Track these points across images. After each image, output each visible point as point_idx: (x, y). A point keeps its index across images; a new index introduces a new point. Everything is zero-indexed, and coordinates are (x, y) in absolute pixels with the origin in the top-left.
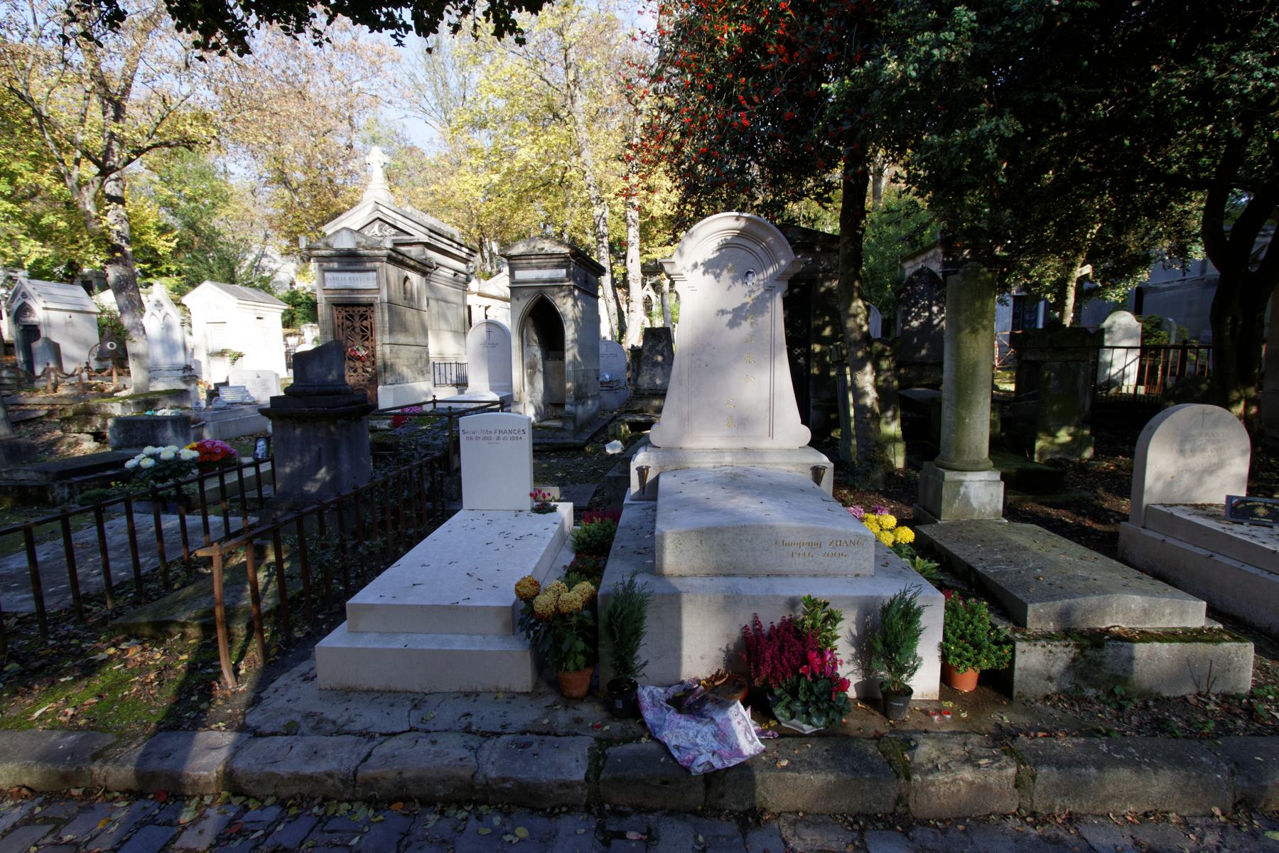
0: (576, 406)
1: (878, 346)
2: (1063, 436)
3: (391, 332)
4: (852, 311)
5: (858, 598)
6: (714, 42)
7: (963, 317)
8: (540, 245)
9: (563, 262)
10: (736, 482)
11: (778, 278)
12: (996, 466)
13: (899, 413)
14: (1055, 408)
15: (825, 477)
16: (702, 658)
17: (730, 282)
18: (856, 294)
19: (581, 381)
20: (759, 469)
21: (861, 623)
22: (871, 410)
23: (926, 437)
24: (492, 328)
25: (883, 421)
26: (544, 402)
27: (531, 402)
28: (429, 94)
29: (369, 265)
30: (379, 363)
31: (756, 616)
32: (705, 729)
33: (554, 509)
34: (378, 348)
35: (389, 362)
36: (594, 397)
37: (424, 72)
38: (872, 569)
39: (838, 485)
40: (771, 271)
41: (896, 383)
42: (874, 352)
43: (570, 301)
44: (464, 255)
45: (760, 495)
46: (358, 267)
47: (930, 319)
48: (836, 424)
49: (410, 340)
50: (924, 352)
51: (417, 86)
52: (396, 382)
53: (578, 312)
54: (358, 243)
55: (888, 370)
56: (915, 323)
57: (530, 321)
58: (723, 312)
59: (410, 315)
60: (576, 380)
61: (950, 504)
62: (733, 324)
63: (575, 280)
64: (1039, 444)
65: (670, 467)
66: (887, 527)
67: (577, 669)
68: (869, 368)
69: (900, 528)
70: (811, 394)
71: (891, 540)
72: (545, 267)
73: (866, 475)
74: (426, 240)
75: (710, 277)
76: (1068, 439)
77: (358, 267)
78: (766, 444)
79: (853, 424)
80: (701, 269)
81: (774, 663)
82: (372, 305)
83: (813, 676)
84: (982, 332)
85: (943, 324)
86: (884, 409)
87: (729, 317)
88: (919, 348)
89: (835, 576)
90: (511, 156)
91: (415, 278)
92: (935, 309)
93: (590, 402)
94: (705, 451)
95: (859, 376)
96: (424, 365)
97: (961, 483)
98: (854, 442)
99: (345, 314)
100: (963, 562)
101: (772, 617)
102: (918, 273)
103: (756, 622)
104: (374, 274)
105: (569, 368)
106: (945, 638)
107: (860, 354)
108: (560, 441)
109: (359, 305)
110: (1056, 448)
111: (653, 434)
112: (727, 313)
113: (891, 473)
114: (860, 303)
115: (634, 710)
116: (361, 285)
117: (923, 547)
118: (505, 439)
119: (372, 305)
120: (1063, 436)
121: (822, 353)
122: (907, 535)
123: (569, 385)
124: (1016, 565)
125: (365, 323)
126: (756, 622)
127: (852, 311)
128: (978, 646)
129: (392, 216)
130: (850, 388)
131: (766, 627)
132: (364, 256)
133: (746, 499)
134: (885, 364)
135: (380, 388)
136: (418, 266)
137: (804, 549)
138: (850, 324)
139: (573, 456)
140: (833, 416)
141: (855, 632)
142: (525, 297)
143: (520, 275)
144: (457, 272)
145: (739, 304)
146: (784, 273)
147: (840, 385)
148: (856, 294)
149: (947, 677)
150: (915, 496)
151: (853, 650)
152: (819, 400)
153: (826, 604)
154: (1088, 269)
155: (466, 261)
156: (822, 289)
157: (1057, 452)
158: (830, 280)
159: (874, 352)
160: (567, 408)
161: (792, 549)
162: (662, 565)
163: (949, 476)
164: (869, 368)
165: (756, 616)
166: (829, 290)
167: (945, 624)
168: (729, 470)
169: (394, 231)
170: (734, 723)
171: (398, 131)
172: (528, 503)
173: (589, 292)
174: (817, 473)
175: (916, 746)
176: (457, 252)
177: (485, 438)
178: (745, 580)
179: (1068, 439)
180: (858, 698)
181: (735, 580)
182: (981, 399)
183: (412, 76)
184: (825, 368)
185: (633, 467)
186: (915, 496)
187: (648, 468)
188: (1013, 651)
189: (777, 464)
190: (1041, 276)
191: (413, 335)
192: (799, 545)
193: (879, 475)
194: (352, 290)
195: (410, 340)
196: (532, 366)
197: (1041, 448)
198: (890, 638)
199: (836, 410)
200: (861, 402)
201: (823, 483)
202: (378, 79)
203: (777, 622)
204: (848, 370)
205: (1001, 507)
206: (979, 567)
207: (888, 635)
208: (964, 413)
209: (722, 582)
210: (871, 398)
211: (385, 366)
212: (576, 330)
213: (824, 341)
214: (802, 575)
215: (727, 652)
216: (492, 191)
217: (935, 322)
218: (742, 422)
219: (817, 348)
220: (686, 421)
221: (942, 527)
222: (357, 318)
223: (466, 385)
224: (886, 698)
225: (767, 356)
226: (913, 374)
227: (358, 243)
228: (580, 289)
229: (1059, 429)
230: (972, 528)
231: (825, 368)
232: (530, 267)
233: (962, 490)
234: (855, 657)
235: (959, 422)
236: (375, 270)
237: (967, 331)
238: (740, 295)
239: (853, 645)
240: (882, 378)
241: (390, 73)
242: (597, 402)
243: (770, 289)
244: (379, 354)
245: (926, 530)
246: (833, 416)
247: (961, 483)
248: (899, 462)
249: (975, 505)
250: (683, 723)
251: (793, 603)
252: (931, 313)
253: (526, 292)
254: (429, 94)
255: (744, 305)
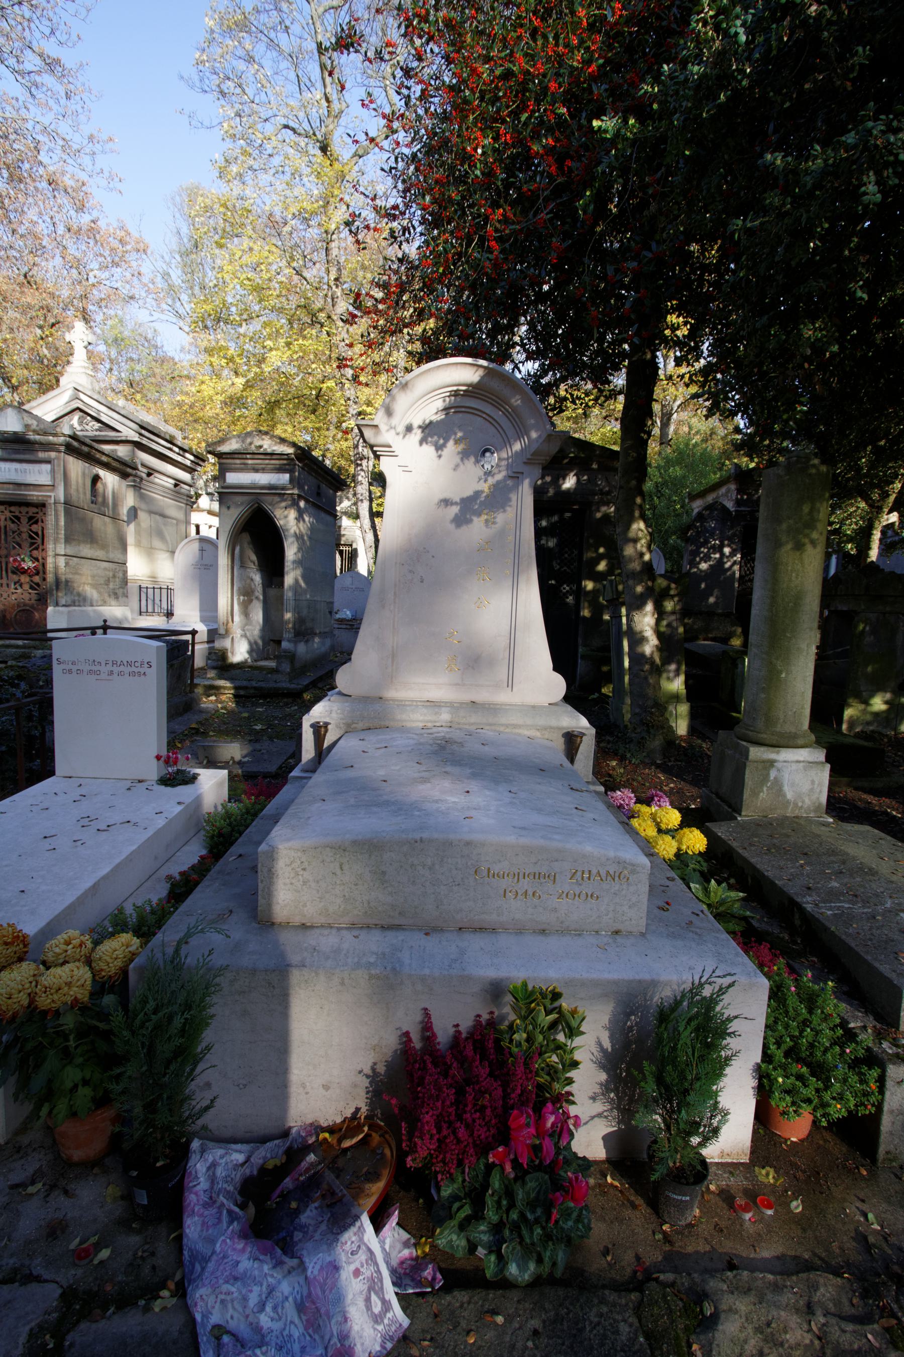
0: (296, 643)
1: (662, 582)
2: (878, 704)
3: (68, 540)
4: (631, 534)
5: (616, 983)
6: (466, 158)
7: (784, 526)
8: (257, 442)
9: (284, 464)
10: (447, 753)
11: (529, 459)
12: (819, 743)
13: (683, 667)
14: (869, 669)
15: (582, 749)
16: (326, 1087)
17: (457, 459)
18: (637, 514)
19: (305, 612)
20: (488, 733)
21: (618, 1029)
22: (651, 660)
23: (719, 697)
24: (206, 546)
25: (664, 675)
26: (262, 638)
27: (244, 636)
28: (184, 297)
29: (41, 455)
30: (50, 577)
31: (426, 1012)
32: (285, 1287)
33: (193, 779)
34: (50, 560)
35: (63, 578)
36: (323, 635)
37: (179, 272)
38: (643, 922)
39: (602, 752)
40: (517, 447)
41: (681, 630)
42: (657, 589)
43: (292, 514)
44: (188, 463)
45: (474, 776)
46: (27, 457)
47: (720, 562)
48: (607, 678)
49: (100, 554)
50: (712, 600)
51: (171, 287)
52: (73, 604)
53: (303, 528)
54: (27, 426)
55: (673, 613)
56: (704, 566)
57: (246, 537)
58: (446, 502)
59: (100, 523)
60: (297, 610)
61: (755, 794)
62: (461, 520)
63: (300, 487)
64: (848, 713)
65: (360, 725)
66: (667, 828)
67: (73, 1114)
68: (649, 607)
69: (686, 830)
70: (580, 641)
71: (673, 851)
72: (263, 470)
73: (641, 743)
74: (136, 438)
75: (429, 450)
76: (884, 707)
77: (27, 457)
78: (503, 697)
79: (627, 678)
80: (417, 435)
81: (458, 1102)
82: (43, 505)
83: (516, 1164)
84: (809, 548)
85: (736, 567)
86: (666, 661)
87: (455, 509)
88: (708, 593)
89: (579, 933)
90: (262, 361)
91: (110, 480)
92: (727, 550)
93: (317, 640)
94: (414, 704)
95: (637, 617)
96: (118, 585)
97: (772, 763)
98: (628, 701)
99: (8, 514)
100: (780, 892)
101: (454, 1016)
102: (709, 507)
103: (427, 1026)
104: (48, 467)
105: (289, 595)
106: (766, 1056)
107: (639, 589)
108: (272, 685)
109: (28, 504)
110: (869, 718)
111: (343, 678)
112: (452, 504)
113: (671, 742)
114: (642, 525)
115: (169, 1207)
116: (31, 479)
117: (720, 862)
118: (120, 674)
119: (43, 505)
120: (878, 704)
121: (595, 592)
122: (695, 841)
123: (288, 616)
124: (866, 902)
125: (35, 528)
126: (427, 1026)
127: (631, 534)
128: (820, 1070)
129: (94, 407)
130: (626, 633)
131: (443, 1033)
132: (34, 443)
133: (447, 784)
134: (669, 605)
135: (50, 609)
136: (115, 464)
137: (525, 884)
138: (629, 551)
139: (286, 704)
140: (605, 669)
141: (607, 1045)
142: (237, 506)
143: (232, 478)
144: (178, 483)
145: (469, 493)
146: (535, 454)
147: (614, 630)
148: (637, 514)
149: (763, 1116)
150: (707, 780)
151: (603, 1076)
152: (579, 644)
153: (556, 996)
154: (894, 518)
155: (191, 470)
156: (599, 515)
157: (868, 723)
158: (607, 504)
159: (657, 589)
160: (285, 645)
161: (504, 883)
162: (269, 905)
163: (756, 753)
164: (649, 607)
165: (426, 1012)
166: (606, 516)
167: (767, 1026)
168: (443, 732)
169: (97, 425)
170: (346, 1273)
171: (150, 336)
172: (152, 770)
173: (324, 510)
174: (571, 741)
175: (715, 1319)
176: (179, 459)
177: (90, 672)
178: (417, 940)
179: (884, 707)
180: (608, 1160)
181: (401, 936)
182: (803, 646)
183: (166, 276)
184: (598, 611)
185: (307, 721)
186: (707, 780)
187: (326, 724)
188: (881, 1081)
189: (515, 726)
190: (842, 522)
191: (104, 547)
192: (517, 876)
193: (656, 743)
194: (19, 485)
195: (100, 554)
196: (247, 594)
197: (851, 717)
198: (670, 1075)
199: (607, 661)
200: (639, 650)
201: (580, 756)
202: (119, 270)
203: (466, 1024)
204: (624, 611)
205: (824, 799)
206: (808, 903)
207: (666, 1054)
208: (779, 665)
209: (375, 942)
210: (651, 646)
211: (58, 582)
212: (300, 549)
213: (597, 577)
214: (520, 931)
215: (373, 1076)
216: (235, 402)
217: (727, 565)
218: (473, 661)
219: (589, 585)
220: (393, 662)
221: (744, 826)
222: (24, 520)
223: (172, 615)
224: (654, 1168)
225: (509, 572)
226: (699, 624)
227: (27, 426)
228: (307, 501)
229: (872, 696)
230: (783, 830)
231: (598, 611)
232: (245, 469)
233: (773, 774)
234: (606, 1088)
235: (772, 679)
236: (48, 462)
237: (789, 546)
238: (472, 479)
239: (602, 1067)
240: (665, 623)
241: (134, 264)
242: (328, 642)
243: (515, 476)
244: (50, 566)
245: (722, 830)
246: (605, 669)
247: (772, 763)
248: (682, 727)
249: (790, 795)
250: (245, 1264)
251: (496, 991)
252: (722, 554)
253: (239, 499)
254: (184, 297)
255: (477, 494)
